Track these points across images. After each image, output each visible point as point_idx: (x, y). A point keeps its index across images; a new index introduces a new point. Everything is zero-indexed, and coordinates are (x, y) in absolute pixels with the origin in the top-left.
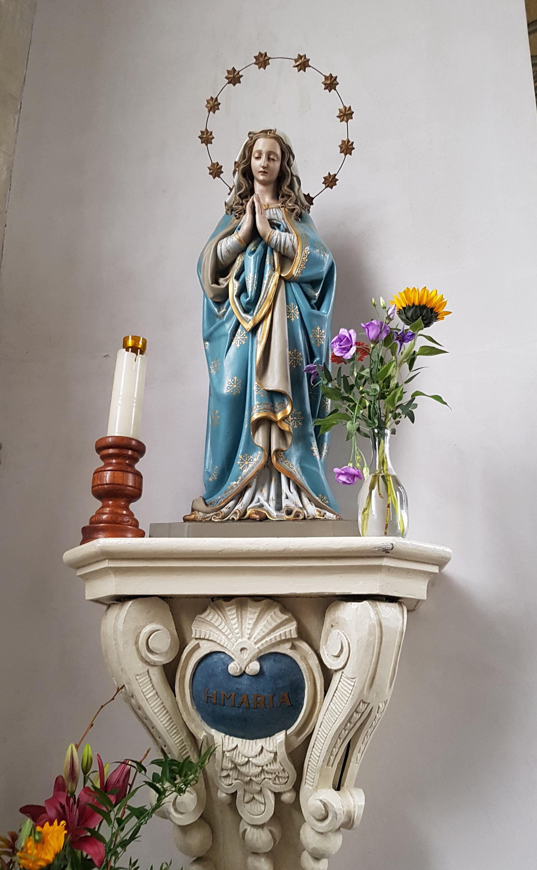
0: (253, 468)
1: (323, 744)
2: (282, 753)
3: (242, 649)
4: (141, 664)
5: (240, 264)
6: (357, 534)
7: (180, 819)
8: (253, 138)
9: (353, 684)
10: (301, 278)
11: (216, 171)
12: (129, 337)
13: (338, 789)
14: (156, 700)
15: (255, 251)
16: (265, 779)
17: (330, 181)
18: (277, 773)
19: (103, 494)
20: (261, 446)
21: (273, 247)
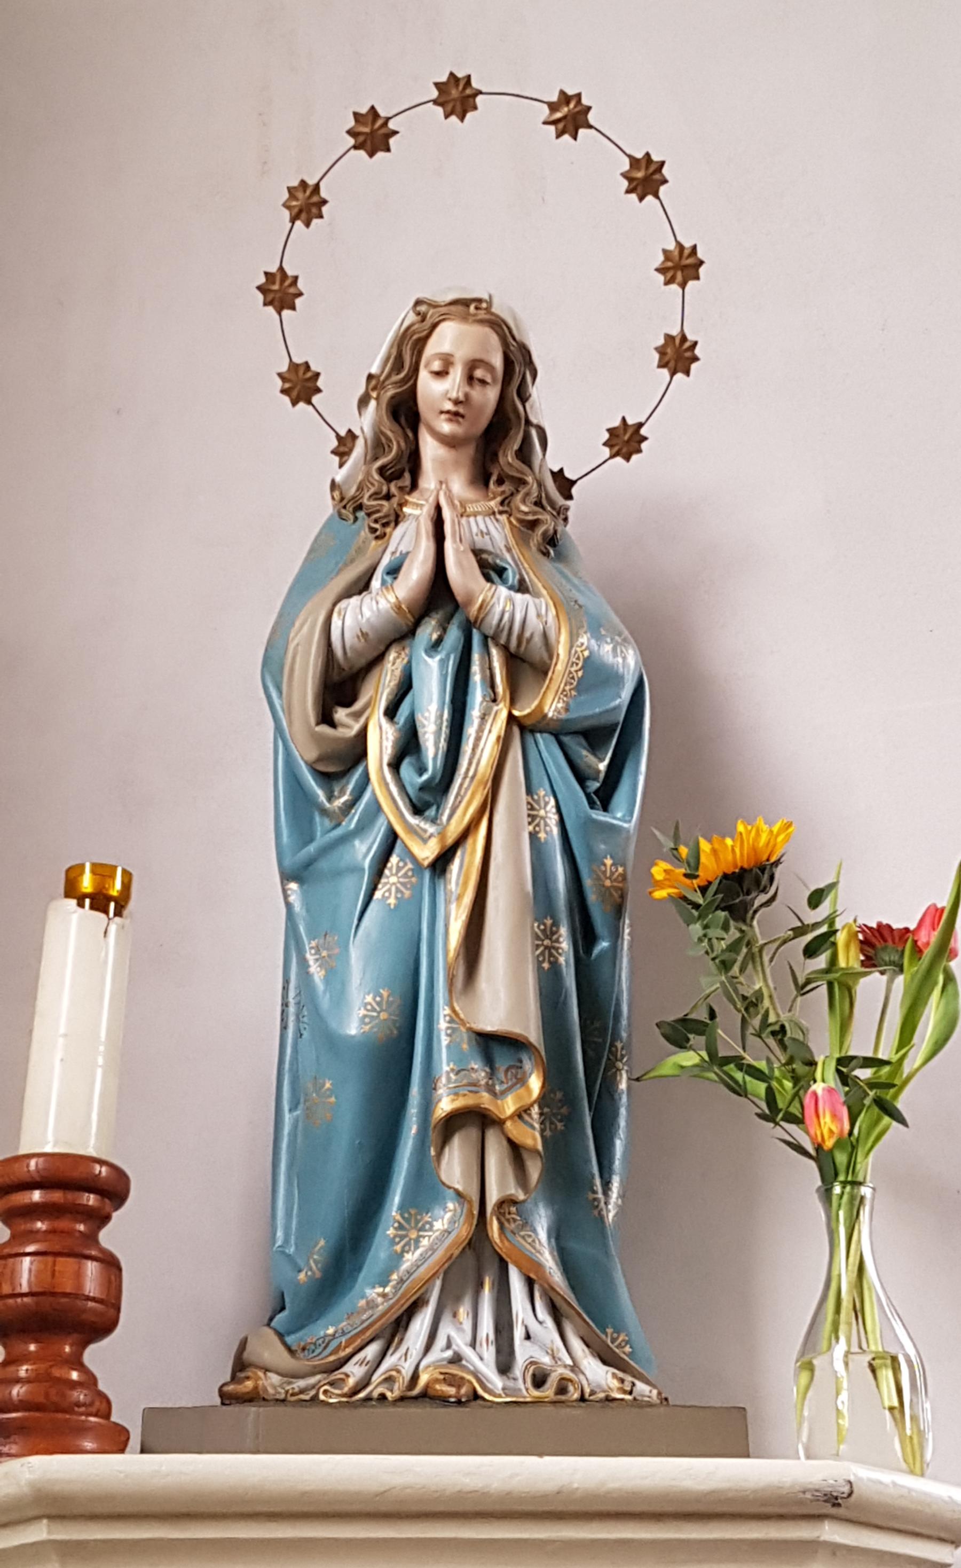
0: (432, 1249)
5: (398, 673)
6: (740, 1448)
8: (427, 318)
12: (82, 866)
17: (626, 441)
21: (490, 632)
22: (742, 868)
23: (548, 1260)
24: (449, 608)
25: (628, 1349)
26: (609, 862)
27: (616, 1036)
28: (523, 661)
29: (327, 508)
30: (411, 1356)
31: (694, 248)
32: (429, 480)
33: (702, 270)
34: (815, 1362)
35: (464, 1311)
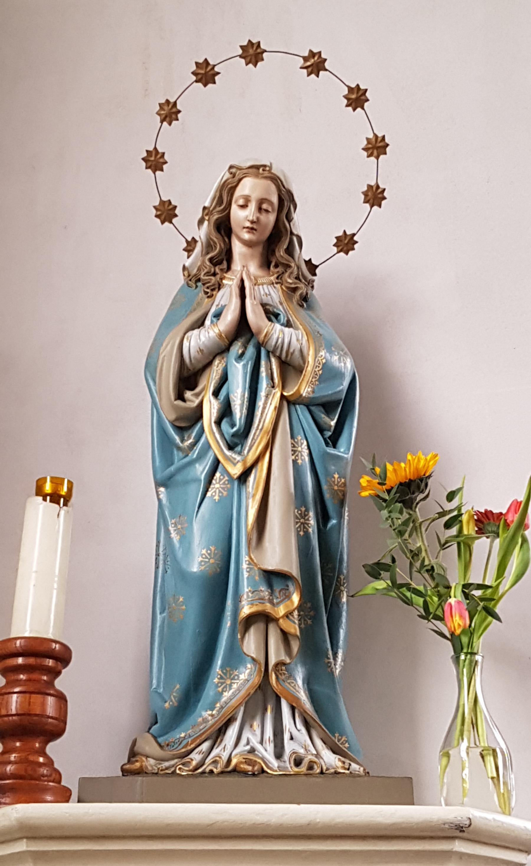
0: (239, 690)
5: (220, 372)
6: (409, 800)
8: (236, 176)
12: (45, 478)
17: (346, 243)
20: (254, 655)
21: (271, 349)
22: (410, 480)
23: (303, 696)
24: (248, 336)
25: (347, 745)
26: (336, 476)
27: (340, 572)
28: (289, 365)
29: (181, 280)
30: (227, 749)
31: (384, 137)
32: (237, 265)
33: (388, 149)
34: (450, 752)
35: (256, 724)
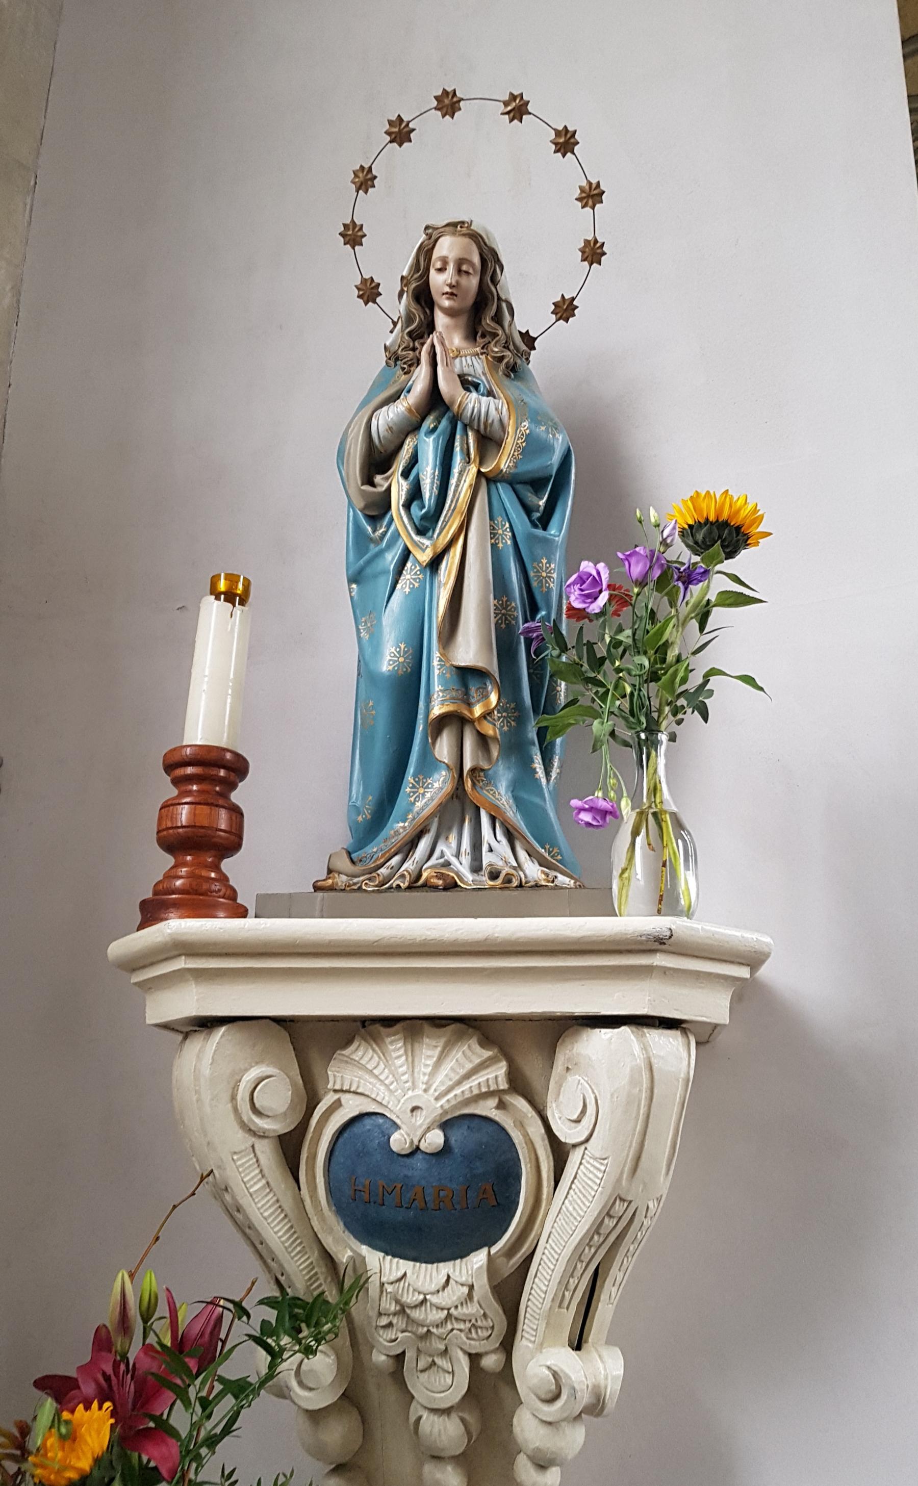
0: (432, 799)
1: (553, 1271)
2: (482, 1286)
3: (414, 1109)
4: (241, 1134)
5: (410, 451)
6: (611, 912)
7: (307, 1399)
8: (432, 235)
9: (603, 1168)
10: (515, 475)
11: (369, 292)
12: (220, 575)
13: (578, 1347)
14: (266, 1196)
15: (435, 429)
16: (452, 1330)
17: (565, 310)
18: (473, 1321)
19: (175, 843)
21: (467, 421)
